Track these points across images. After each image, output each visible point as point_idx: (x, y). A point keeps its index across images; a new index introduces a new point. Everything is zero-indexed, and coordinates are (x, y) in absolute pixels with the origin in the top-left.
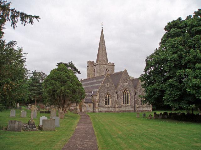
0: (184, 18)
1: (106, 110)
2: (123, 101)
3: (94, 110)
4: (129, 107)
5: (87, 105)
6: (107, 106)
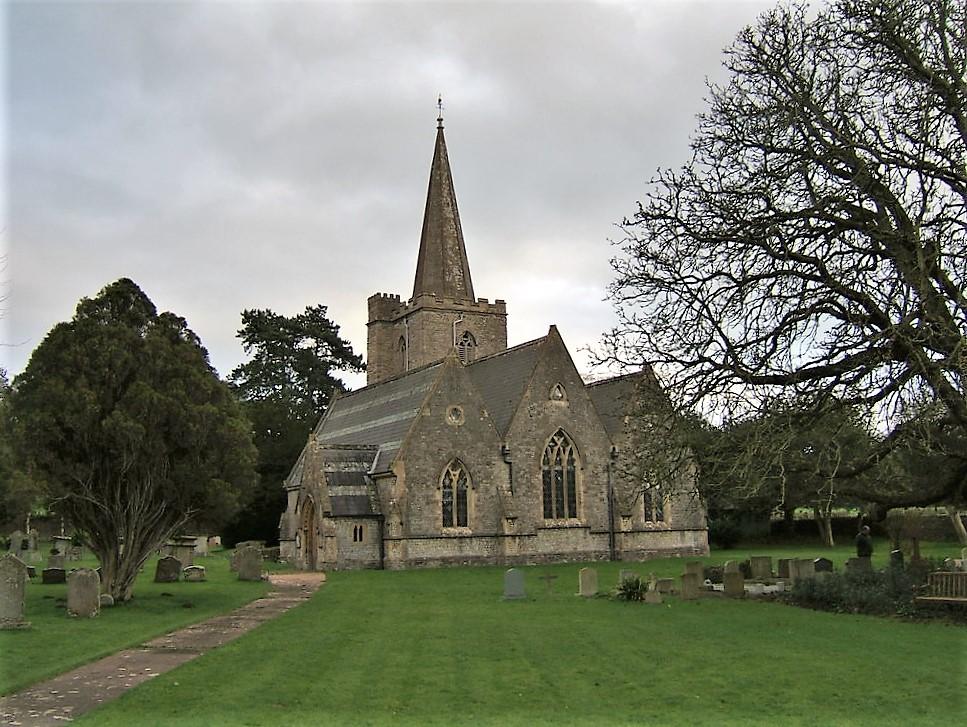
0: (812, 610)
1: (448, 550)
2: (547, 503)
3: (383, 555)
4: (581, 533)
5: (345, 529)
6: (452, 531)
